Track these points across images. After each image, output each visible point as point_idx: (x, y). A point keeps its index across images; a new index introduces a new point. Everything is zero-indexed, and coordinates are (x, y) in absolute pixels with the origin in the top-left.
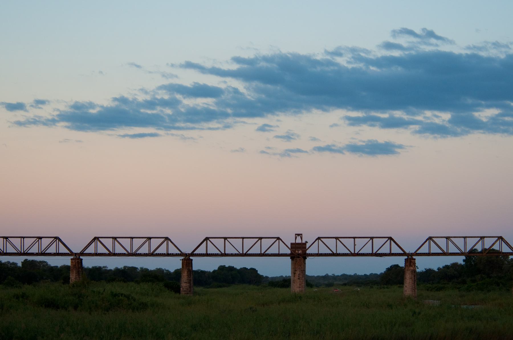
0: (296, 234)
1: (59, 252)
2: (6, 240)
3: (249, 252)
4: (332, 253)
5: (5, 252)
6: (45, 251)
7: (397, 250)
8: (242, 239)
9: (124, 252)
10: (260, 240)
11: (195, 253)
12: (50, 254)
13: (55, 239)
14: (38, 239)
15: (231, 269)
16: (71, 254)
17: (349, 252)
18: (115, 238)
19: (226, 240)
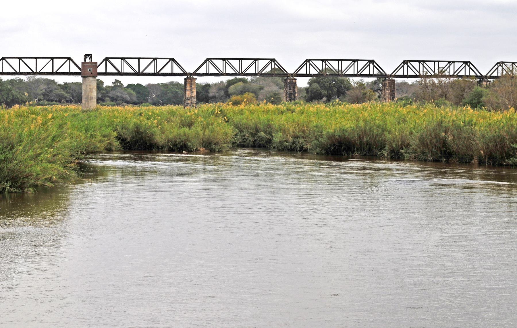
1: (174, 72)
2: (226, 62)
4: (15, 72)
6: (361, 73)
7: (179, 71)
16: (184, 74)
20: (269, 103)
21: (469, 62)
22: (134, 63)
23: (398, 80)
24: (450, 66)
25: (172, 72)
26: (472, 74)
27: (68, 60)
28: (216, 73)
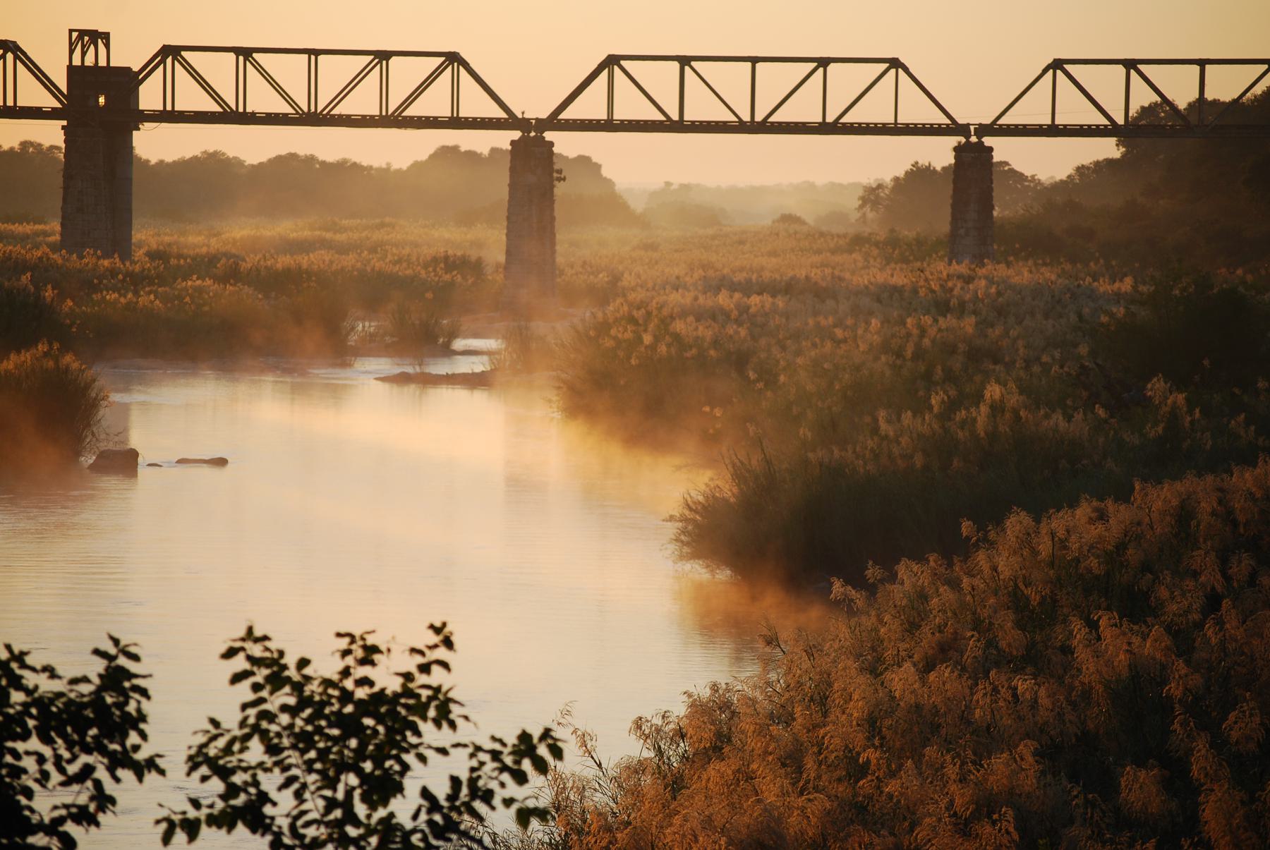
0: (71, 31)
3: (846, 119)
8: (749, 65)
9: (284, 108)
10: (821, 70)
11: (563, 116)
13: (377, 60)
17: (660, 117)
18: (245, 53)
19: (687, 68)
22: (291, 72)
27: (1059, 72)
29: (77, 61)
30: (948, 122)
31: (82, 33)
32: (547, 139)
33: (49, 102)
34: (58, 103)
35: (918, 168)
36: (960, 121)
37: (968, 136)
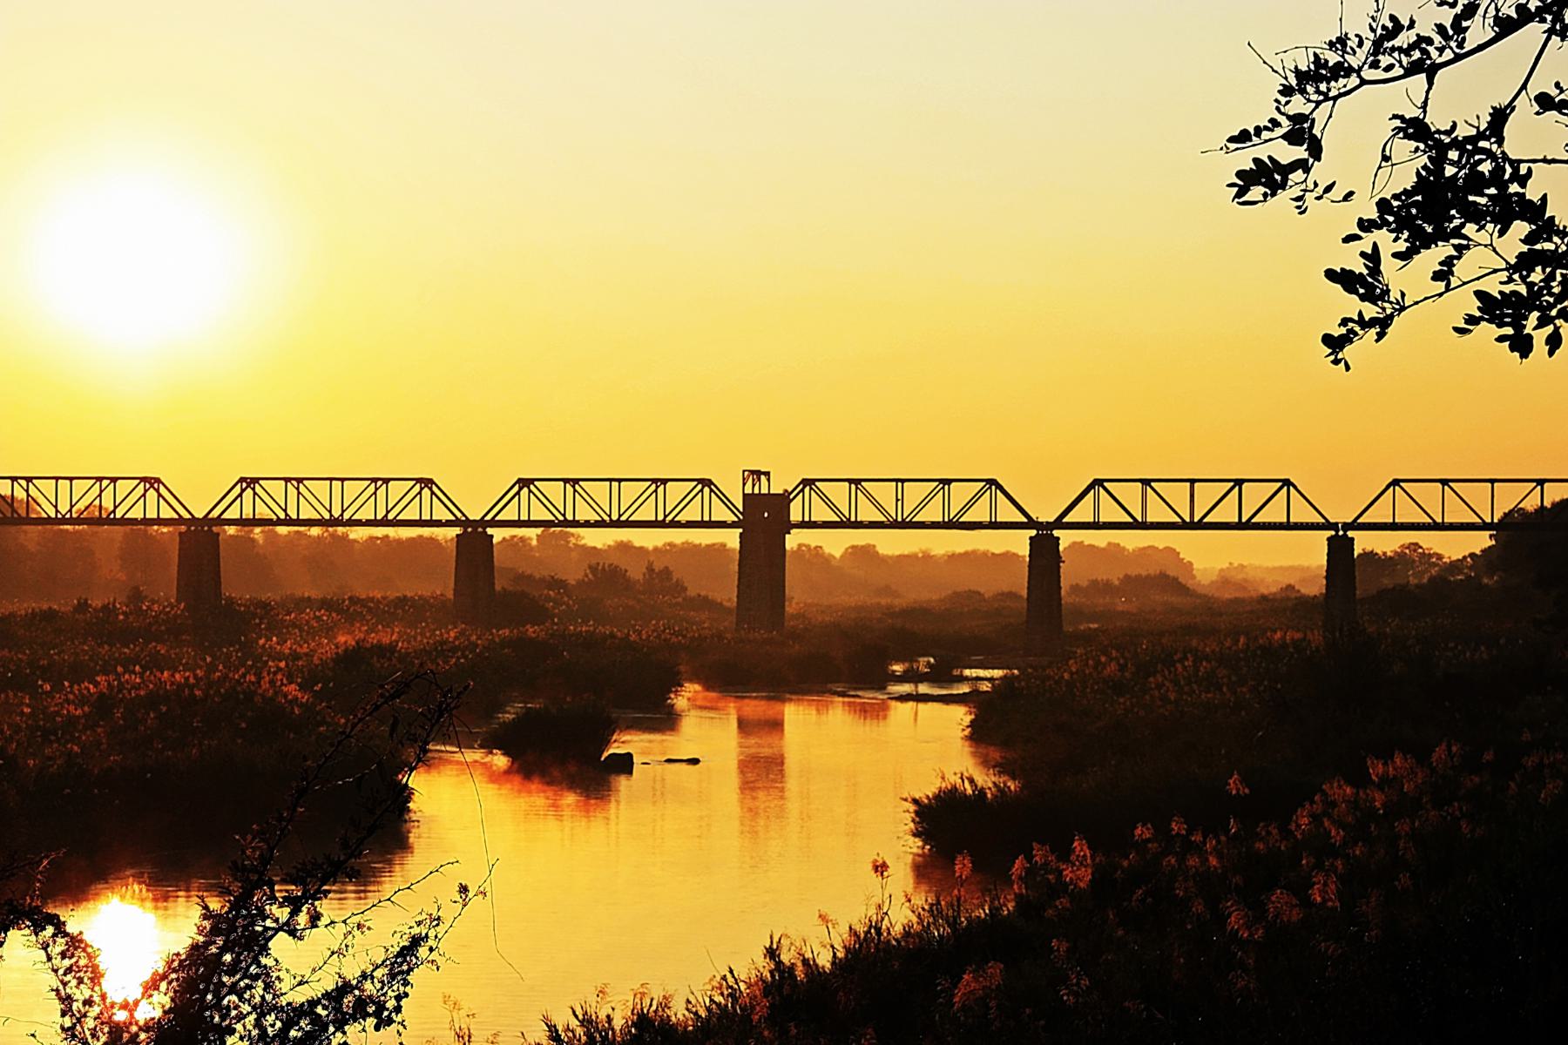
0: (744, 471)
2: (857, 488)
5: (853, 519)
12: (359, 523)
13: (988, 486)
14: (941, 486)
15: (927, 557)
16: (1031, 523)
20: (1068, 628)
21: (158, 481)
22: (885, 493)
23: (498, 534)
24: (656, 491)
25: (993, 520)
26: (167, 513)
28: (1174, 523)
29: (748, 490)
30: (1323, 521)
31: (752, 472)
32: (1055, 535)
33: (731, 518)
34: (1070, 520)
35: (1365, 553)
36: (1332, 521)
37: (1337, 531)
